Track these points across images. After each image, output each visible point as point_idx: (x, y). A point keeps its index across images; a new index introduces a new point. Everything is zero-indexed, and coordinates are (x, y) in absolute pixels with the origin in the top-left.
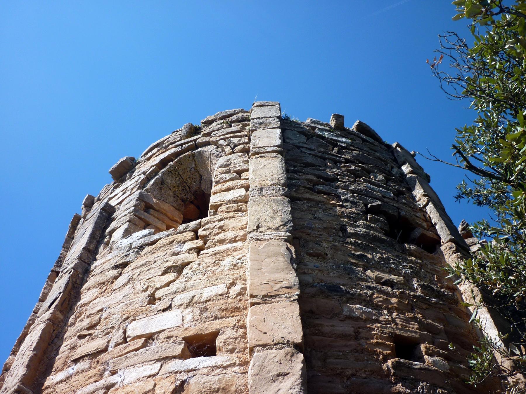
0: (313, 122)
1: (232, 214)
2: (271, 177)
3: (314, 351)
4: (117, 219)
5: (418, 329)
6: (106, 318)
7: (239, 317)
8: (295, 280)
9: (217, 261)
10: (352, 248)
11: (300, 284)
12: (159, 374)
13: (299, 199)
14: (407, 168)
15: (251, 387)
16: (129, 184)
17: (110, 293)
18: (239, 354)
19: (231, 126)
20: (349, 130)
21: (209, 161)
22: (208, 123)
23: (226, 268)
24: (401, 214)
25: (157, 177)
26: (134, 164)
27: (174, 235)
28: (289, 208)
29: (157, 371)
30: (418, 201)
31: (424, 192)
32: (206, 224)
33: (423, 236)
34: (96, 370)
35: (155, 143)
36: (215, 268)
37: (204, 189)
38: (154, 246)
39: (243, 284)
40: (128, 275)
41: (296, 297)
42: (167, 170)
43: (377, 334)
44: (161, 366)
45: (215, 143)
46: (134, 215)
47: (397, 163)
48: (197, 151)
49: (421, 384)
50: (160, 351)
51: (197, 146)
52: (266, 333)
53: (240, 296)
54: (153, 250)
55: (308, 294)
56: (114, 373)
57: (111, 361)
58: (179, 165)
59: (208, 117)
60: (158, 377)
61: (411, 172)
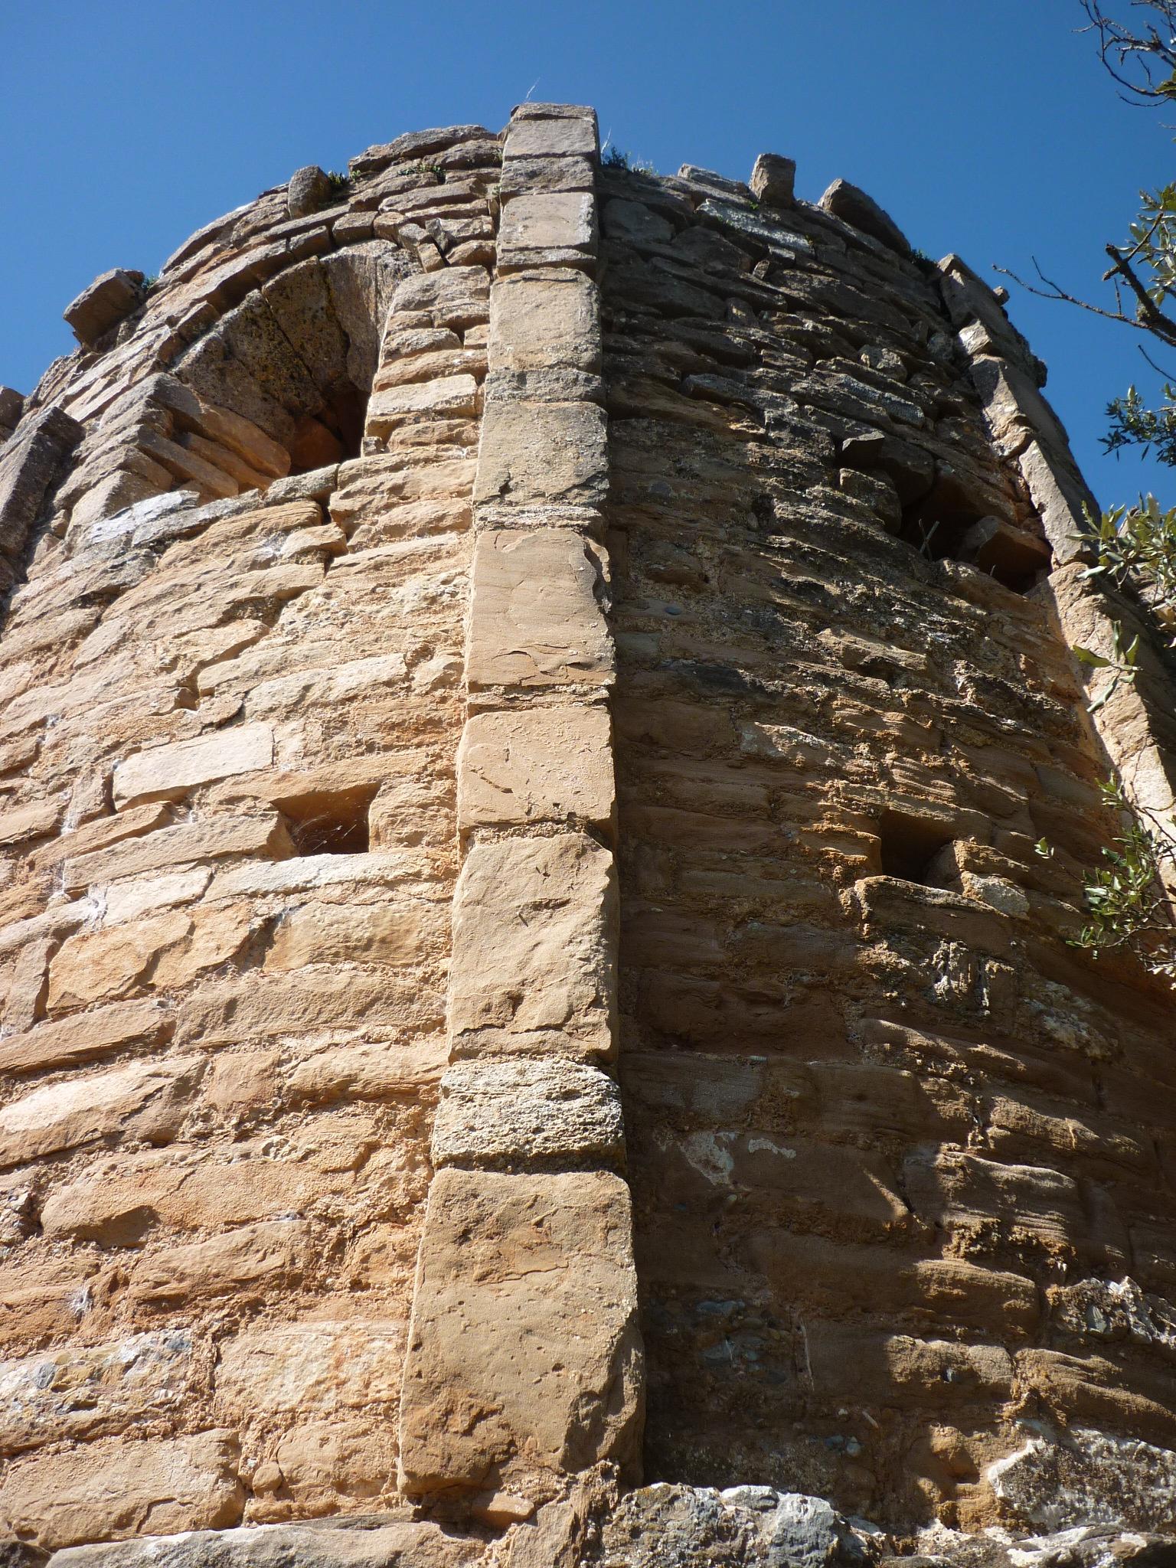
0: (699, 179)
1: (431, 451)
2: (554, 343)
3: (647, 849)
4: (88, 460)
5: (953, 799)
6: (55, 746)
7: (436, 748)
8: (602, 645)
9: (380, 585)
10: (782, 564)
11: (618, 656)
12: (204, 900)
13: (636, 413)
14: (976, 335)
15: (459, 935)
16: (127, 353)
17: (67, 676)
18: (431, 850)
19: (441, 181)
20: (807, 208)
21: (373, 289)
22: (372, 168)
23: (407, 609)
24: (942, 473)
25: (212, 334)
26: (141, 293)
27: (257, 508)
28: (601, 438)
29: (198, 890)
30: (999, 437)
31: (1019, 409)
32: (353, 478)
33: (1000, 539)
34: (28, 886)
35: (207, 228)
36: (375, 607)
37: (357, 377)
38: (195, 542)
39: (454, 654)
40: (118, 623)
41: (605, 693)
42: (241, 315)
43: (832, 808)
44: (211, 878)
45: (391, 233)
46: (141, 450)
47: (949, 319)
48: (334, 256)
49: (944, 946)
50: (207, 837)
51: (334, 241)
52: (509, 791)
53: (444, 687)
54: (193, 553)
55: (641, 687)
56: (76, 894)
57: (69, 863)
58: (280, 299)
59: (371, 149)
60: (201, 905)
61: (987, 349)
